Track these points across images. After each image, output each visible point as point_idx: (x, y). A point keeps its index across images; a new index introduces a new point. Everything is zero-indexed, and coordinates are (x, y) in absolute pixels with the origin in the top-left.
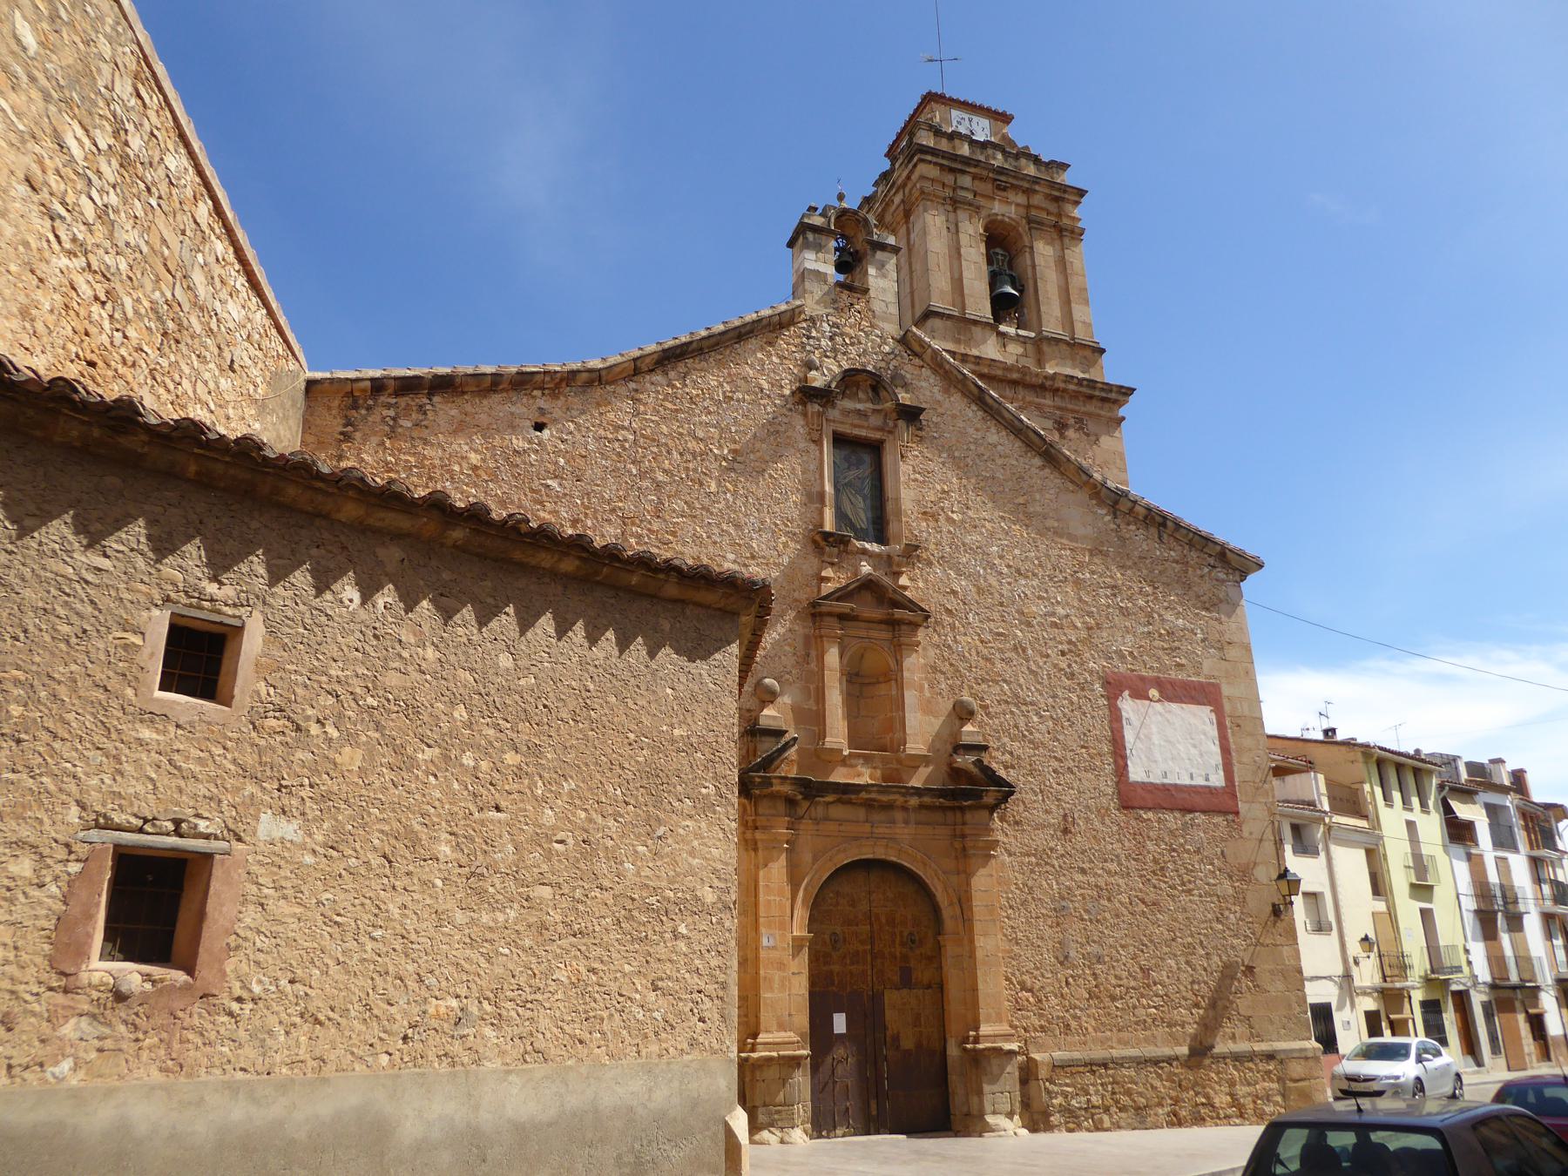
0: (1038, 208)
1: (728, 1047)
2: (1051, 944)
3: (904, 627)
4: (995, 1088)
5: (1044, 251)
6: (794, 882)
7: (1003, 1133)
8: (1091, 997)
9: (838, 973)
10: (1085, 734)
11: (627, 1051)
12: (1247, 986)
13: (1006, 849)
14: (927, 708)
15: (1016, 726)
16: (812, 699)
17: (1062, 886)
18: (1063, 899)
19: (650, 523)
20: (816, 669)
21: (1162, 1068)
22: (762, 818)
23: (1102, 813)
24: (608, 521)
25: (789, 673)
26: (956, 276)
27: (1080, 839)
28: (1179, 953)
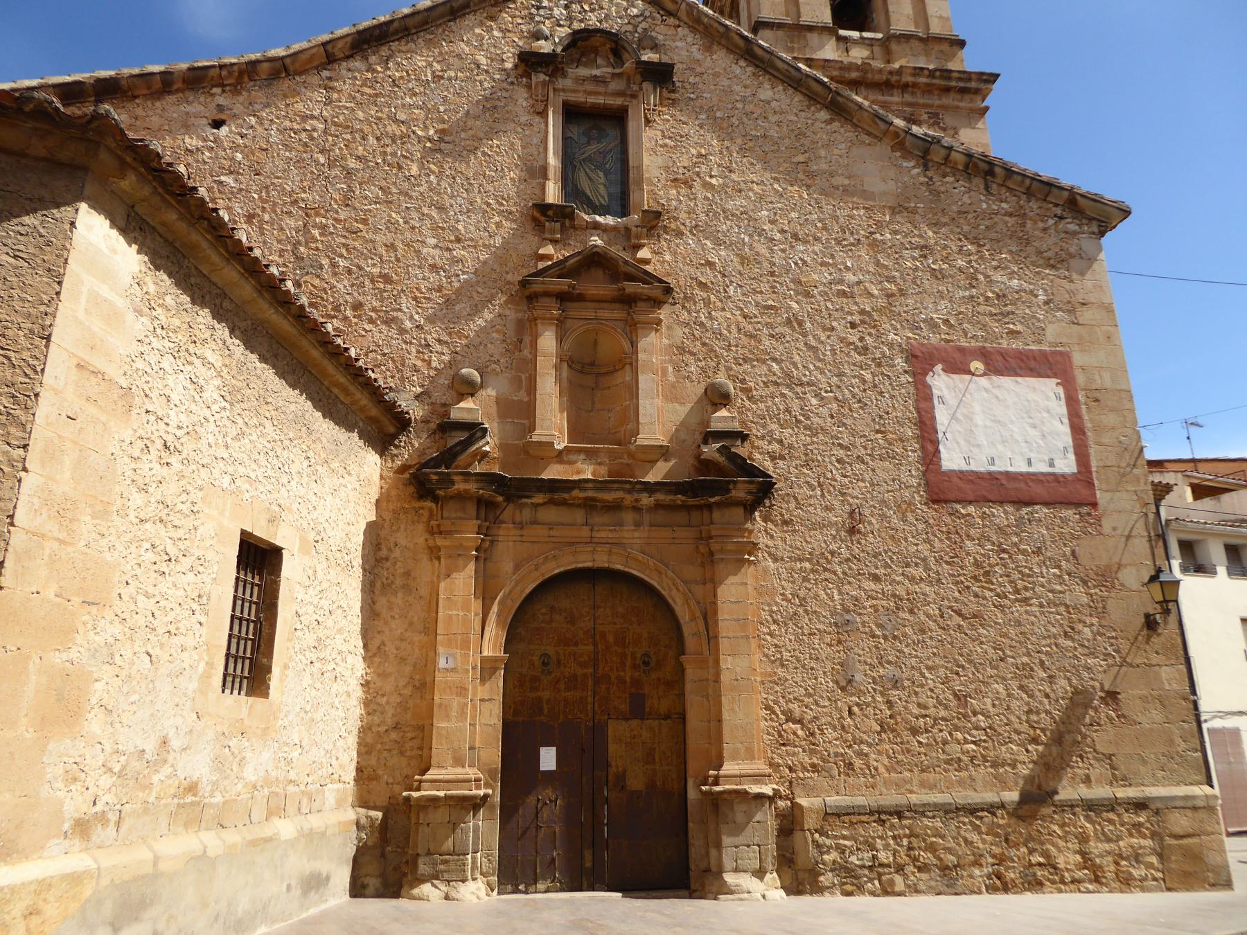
2: (829, 665)
6: (486, 593)
7: (746, 895)
8: (883, 730)
9: (548, 701)
10: (881, 417)
12: (1108, 716)
13: (770, 554)
14: (672, 395)
15: (788, 410)
16: (523, 391)
17: (846, 597)
18: (848, 611)
19: (337, 212)
20: (530, 356)
22: (448, 522)
23: (904, 509)
24: (289, 213)
27: (872, 540)
28: (1010, 675)
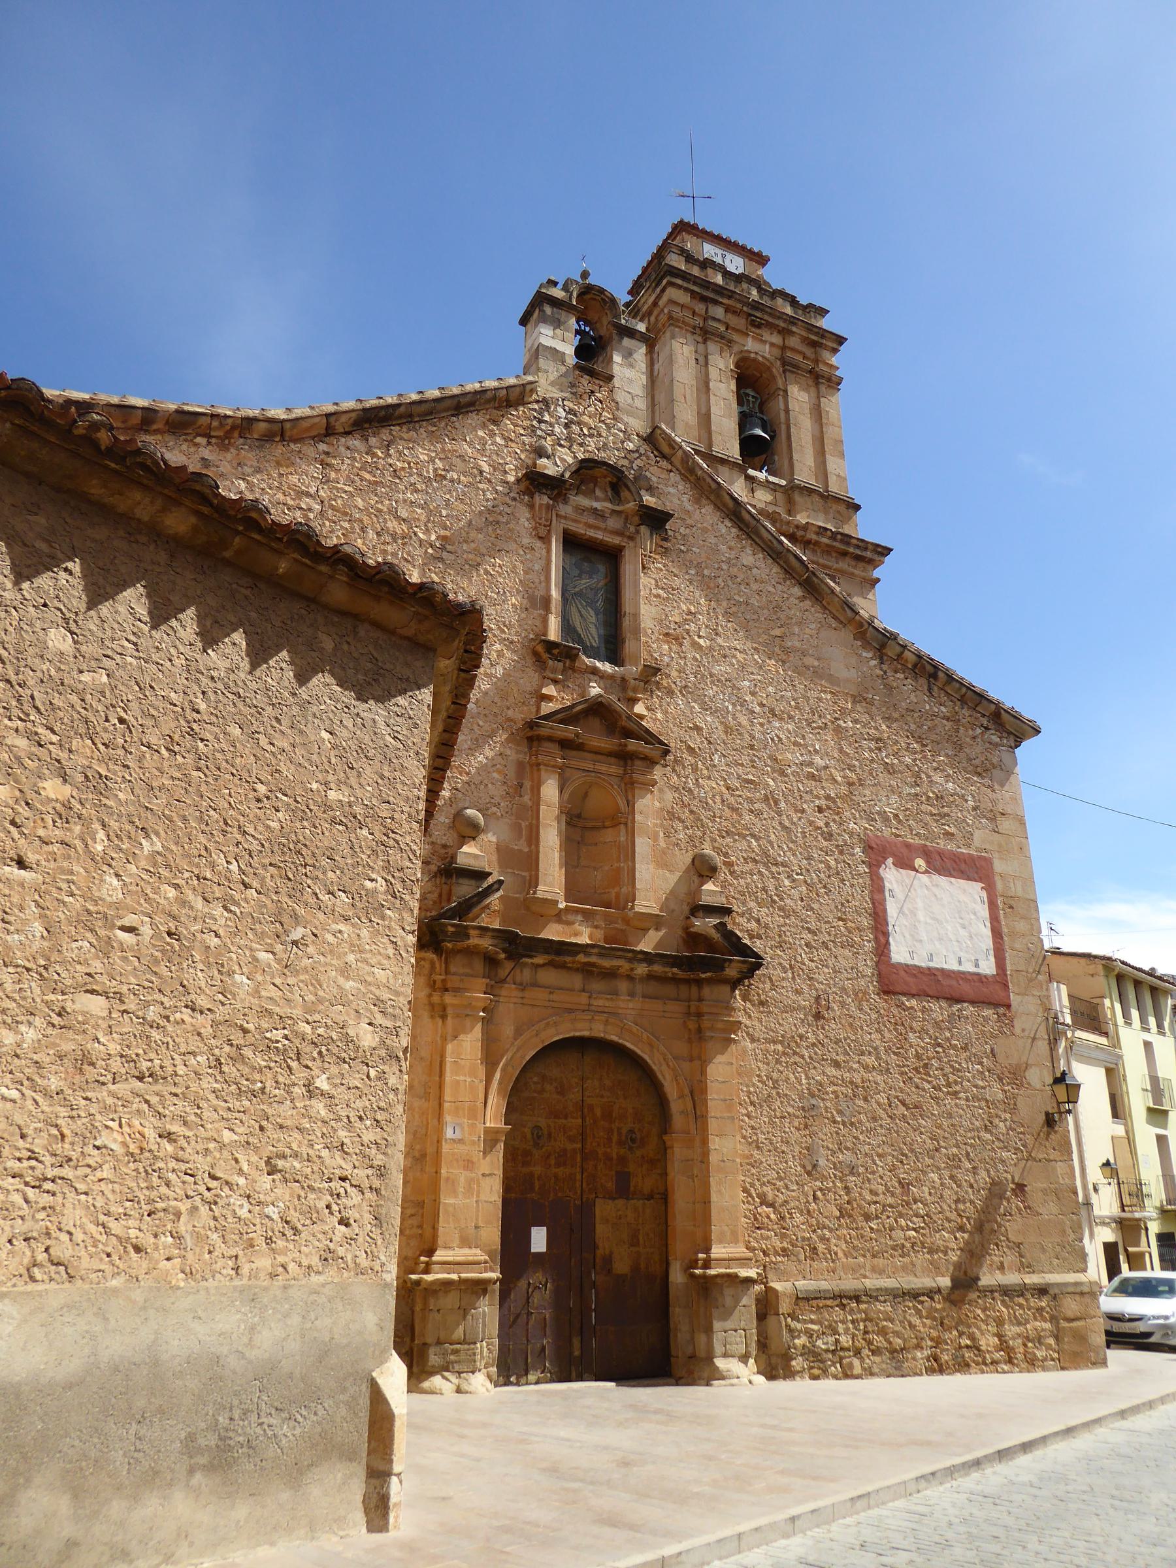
0: (793, 350)
1: (383, 1265)
2: (797, 1149)
3: (638, 763)
4: (729, 1324)
5: (798, 397)
6: (490, 1059)
7: (735, 1381)
8: (842, 1216)
10: (842, 905)
11: (218, 1267)
13: (748, 1034)
14: (662, 861)
15: (764, 889)
17: (812, 1081)
20: (530, 803)
21: (922, 1303)
23: (860, 996)
25: (498, 805)
26: (704, 411)
27: (834, 1026)
